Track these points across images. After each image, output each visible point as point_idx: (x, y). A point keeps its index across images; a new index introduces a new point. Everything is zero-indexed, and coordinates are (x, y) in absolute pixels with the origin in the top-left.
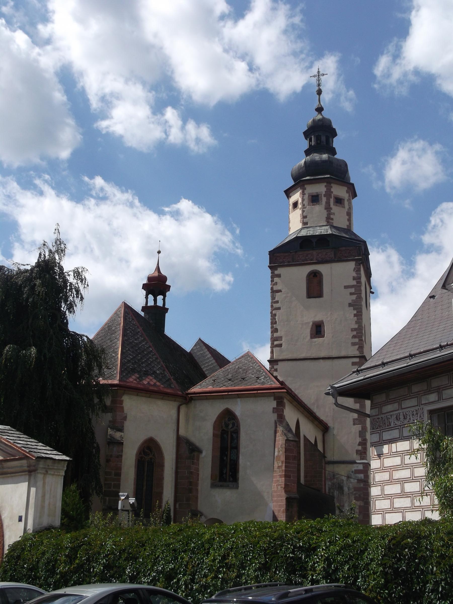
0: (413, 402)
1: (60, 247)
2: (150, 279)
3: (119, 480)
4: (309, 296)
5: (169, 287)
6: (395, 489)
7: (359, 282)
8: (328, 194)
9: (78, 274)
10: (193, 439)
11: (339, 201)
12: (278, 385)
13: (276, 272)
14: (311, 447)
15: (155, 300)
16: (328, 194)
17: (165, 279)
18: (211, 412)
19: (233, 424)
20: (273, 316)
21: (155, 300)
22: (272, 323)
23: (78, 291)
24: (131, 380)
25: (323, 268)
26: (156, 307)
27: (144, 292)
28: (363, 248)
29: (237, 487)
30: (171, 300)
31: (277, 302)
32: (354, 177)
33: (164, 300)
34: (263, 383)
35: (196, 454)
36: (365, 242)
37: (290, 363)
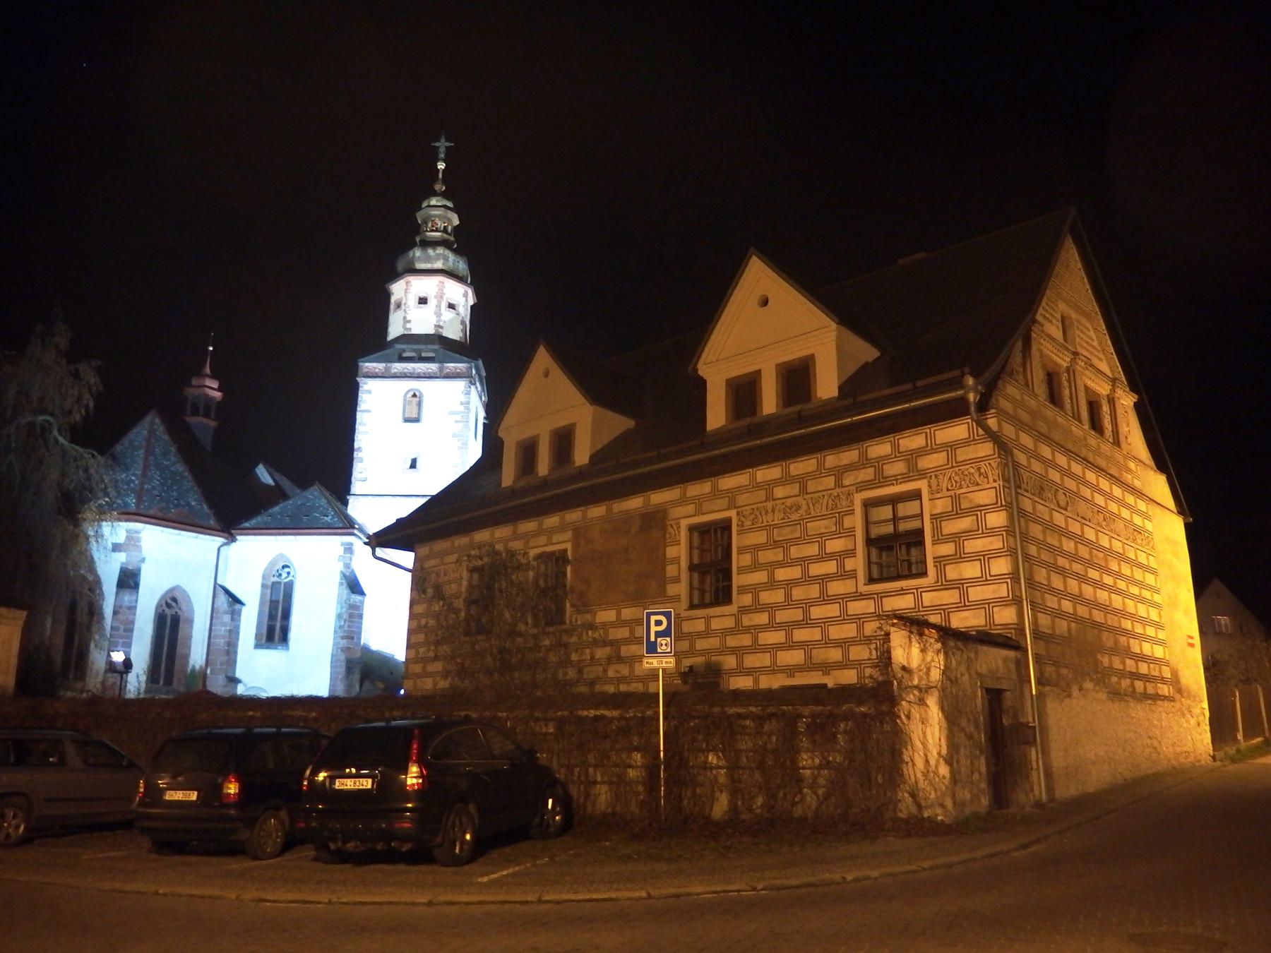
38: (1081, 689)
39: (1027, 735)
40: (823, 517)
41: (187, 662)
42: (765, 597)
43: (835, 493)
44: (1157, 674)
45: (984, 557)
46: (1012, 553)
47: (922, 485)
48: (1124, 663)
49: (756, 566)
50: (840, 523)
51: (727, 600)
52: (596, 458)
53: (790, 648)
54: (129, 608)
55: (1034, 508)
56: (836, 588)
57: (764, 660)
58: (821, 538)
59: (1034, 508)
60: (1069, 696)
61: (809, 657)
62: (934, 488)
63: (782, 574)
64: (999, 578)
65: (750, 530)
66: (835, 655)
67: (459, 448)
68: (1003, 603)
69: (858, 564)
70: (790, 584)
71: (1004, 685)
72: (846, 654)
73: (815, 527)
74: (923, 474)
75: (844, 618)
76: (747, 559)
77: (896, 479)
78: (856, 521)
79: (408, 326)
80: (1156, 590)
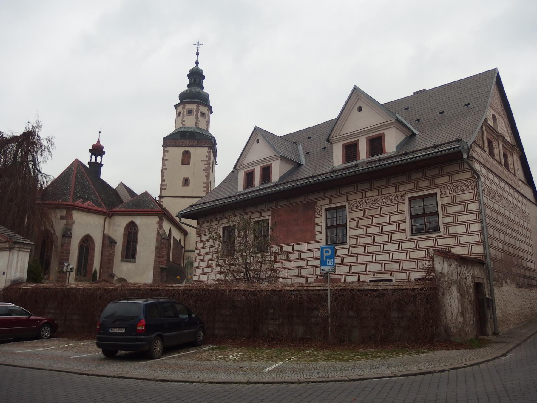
0: (217, 222)
1: (39, 127)
2: (94, 146)
3: (68, 256)
4: (183, 164)
5: (104, 152)
6: (204, 264)
7: (209, 159)
8: (197, 110)
9: (48, 140)
10: (112, 236)
11: (203, 114)
12: (160, 210)
13: (166, 149)
14: (177, 243)
15: (96, 159)
16: (197, 110)
17: (102, 148)
18: (122, 222)
19: (135, 229)
20: (163, 173)
21: (96, 159)
22: (162, 177)
23: (49, 151)
24: (78, 202)
25: (191, 150)
26: (96, 162)
27: (90, 154)
28: (213, 141)
29: (135, 262)
30: (105, 160)
31: (166, 166)
32: (212, 102)
33: (101, 159)
34: (153, 208)
35: (113, 244)
36: (214, 138)
37: (169, 198)
38: (506, 282)
39: (490, 303)
40: (390, 205)
41: (92, 267)
42: (363, 241)
43: (395, 194)
44: (532, 276)
45: (467, 224)
46: (481, 222)
47: (437, 191)
48: (520, 271)
49: (358, 227)
50: (398, 208)
51: (345, 243)
52: (281, 179)
53: (374, 263)
54: (68, 244)
55: (488, 202)
56: (396, 237)
57: (362, 268)
58: (389, 215)
59: (488, 202)
60: (502, 286)
61: (383, 267)
62: (443, 192)
63: (370, 231)
64: (474, 233)
65: (355, 211)
66: (396, 266)
67: (206, 176)
68: (476, 244)
69: (406, 226)
70: (374, 235)
71: (481, 281)
72: (401, 266)
73: (385, 210)
74: (437, 186)
75: (400, 250)
76: (353, 224)
77: (424, 188)
78: (405, 207)
79: (184, 123)
80: (531, 239)
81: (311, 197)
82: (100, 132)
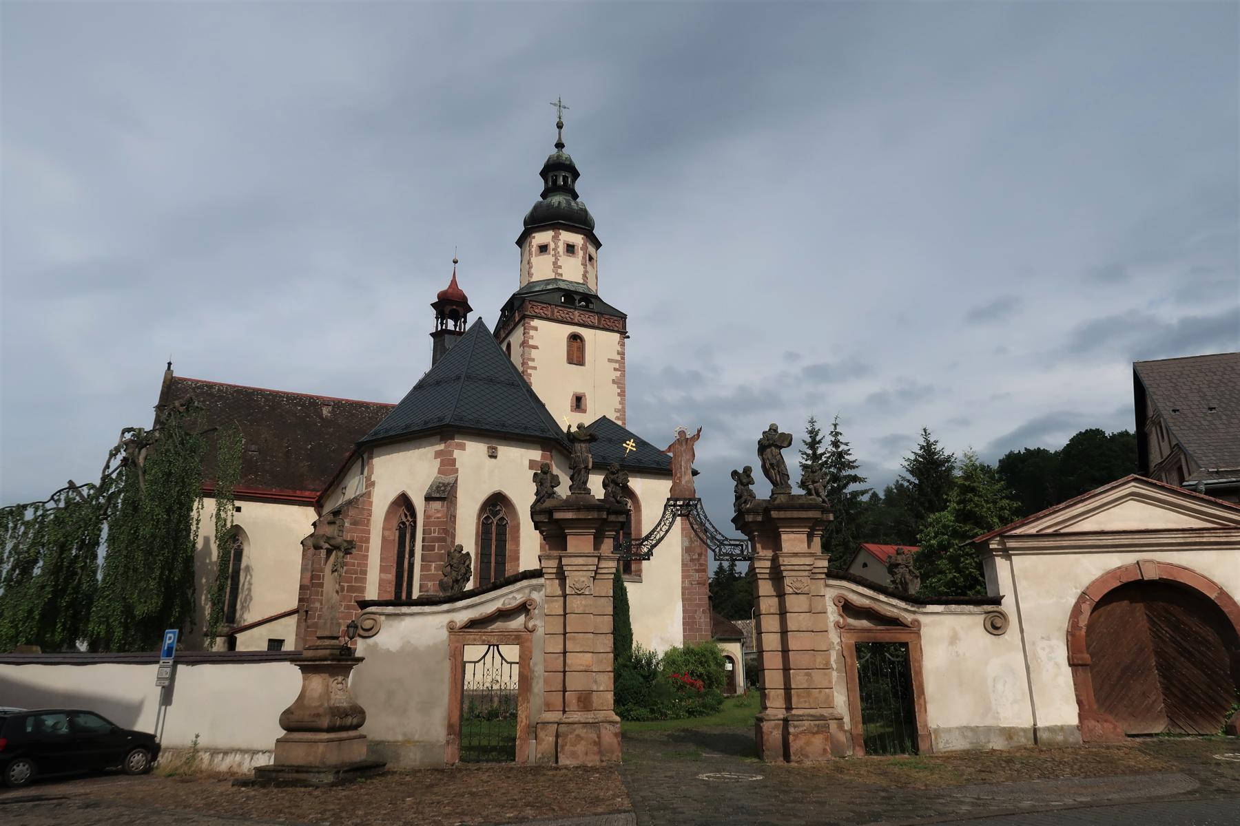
4: (570, 361)
79: (560, 271)
81: (243, 565)
82: (455, 262)
